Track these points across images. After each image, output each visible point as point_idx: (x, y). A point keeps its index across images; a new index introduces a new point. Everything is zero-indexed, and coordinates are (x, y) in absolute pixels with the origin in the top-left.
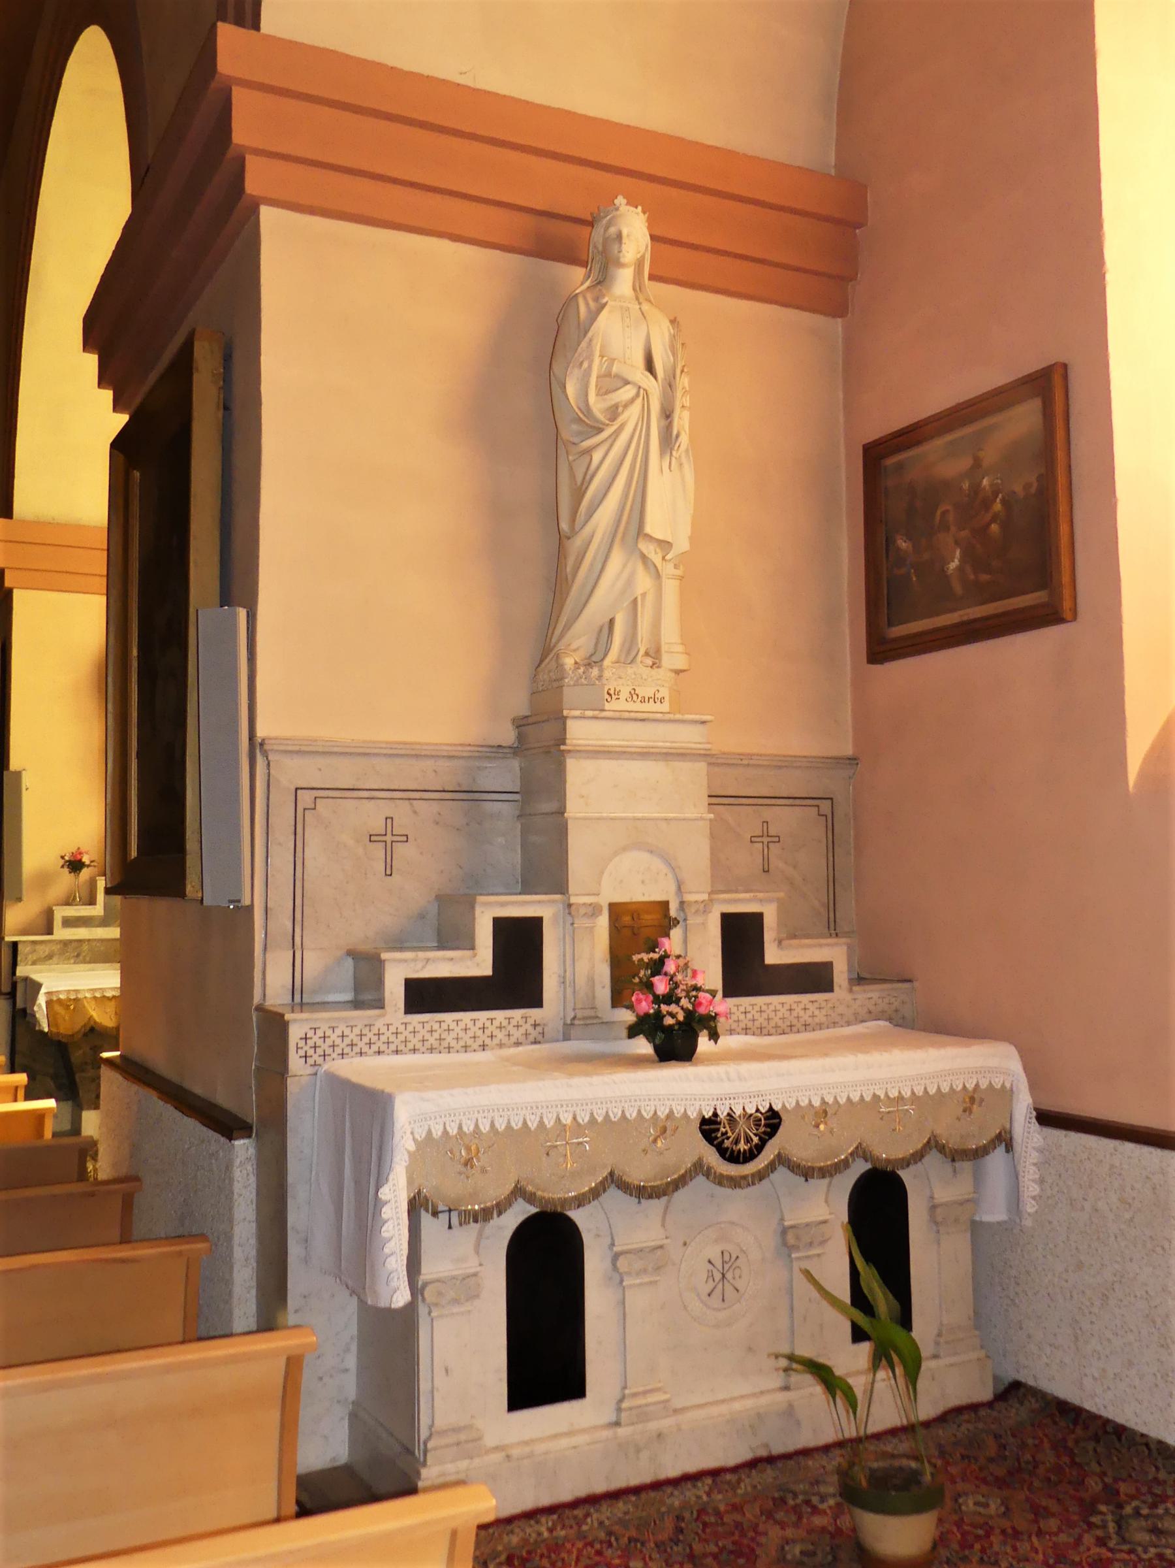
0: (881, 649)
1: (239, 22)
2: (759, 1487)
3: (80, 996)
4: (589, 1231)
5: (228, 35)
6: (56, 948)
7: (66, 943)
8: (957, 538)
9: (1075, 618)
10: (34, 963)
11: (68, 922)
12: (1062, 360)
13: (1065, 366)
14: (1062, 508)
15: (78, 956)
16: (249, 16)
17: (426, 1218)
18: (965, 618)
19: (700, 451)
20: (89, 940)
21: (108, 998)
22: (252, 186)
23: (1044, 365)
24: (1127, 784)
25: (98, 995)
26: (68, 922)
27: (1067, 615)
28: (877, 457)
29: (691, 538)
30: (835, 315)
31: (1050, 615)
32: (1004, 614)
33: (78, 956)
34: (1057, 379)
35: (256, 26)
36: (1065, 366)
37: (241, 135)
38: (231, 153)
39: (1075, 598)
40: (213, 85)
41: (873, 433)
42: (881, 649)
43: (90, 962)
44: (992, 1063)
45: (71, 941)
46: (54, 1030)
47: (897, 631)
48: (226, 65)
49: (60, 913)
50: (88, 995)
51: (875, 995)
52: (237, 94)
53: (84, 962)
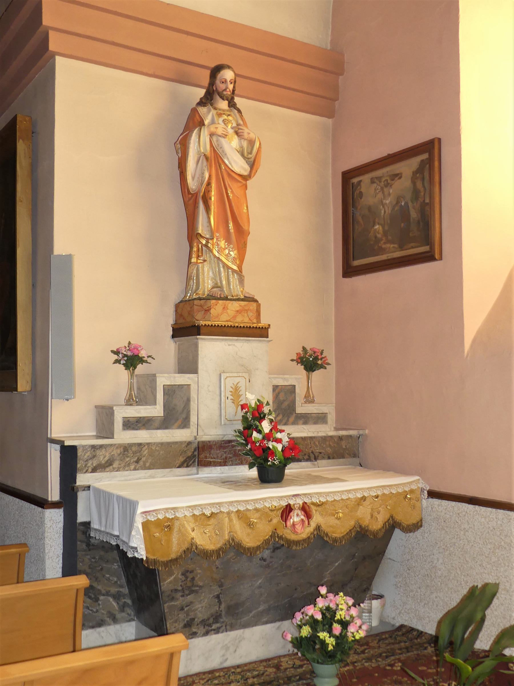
0: (349, 271)
3: (179, 515)
4: (243, 633)
6: (116, 452)
7: (126, 448)
8: (393, 215)
9: (441, 259)
10: (94, 470)
11: (131, 424)
13: (439, 140)
15: (137, 462)
18: (389, 258)
19: (281, 172)
20: (148, 444)
21: (324, 539)
23: (433, 138)
25: (197, 513)
26: (131, 424)
27: (437, 256)
30: (329, 117)
31: (429, 257)
32: (406, 256)
33: (137, 462)
38: (47, 55)
40: (40, 29)
42: (349, 271)
43: (149, 468)
45: (131, 445)
46: (151, 557)
49: (123, 412)
50: (188, 514)
52: (51, 34)
53: (144, 468)
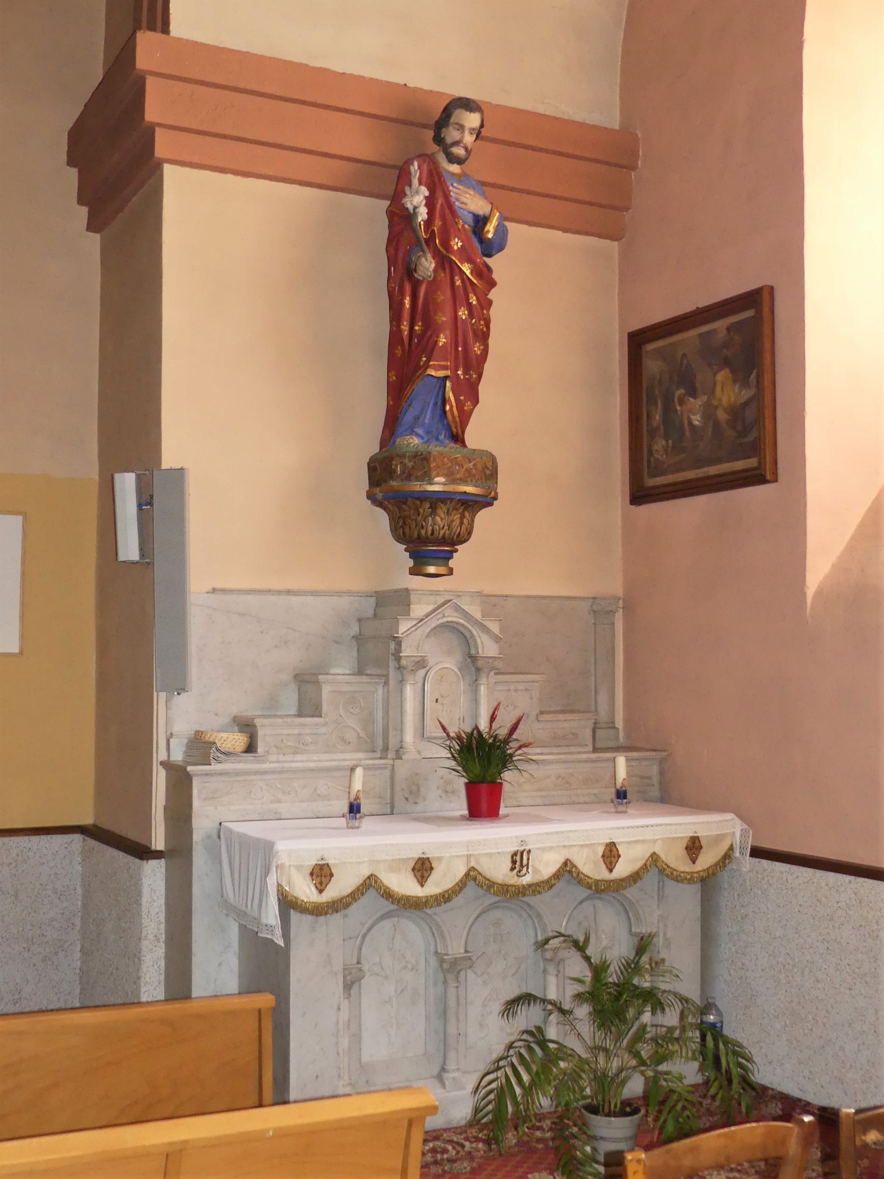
0: (640, 495)
1: (152, 28)
2: (225, 912)
5: (145, 40)
12: (769, 283)
13: (772, 288)
14: (767, 346)
16: (160, 21)
17: (294, 915)
22: (160, 151)
24: (806, 601)
28: (637, 341)
29: (427, 213)
31: (756, 477)
34: (765, 293)
35: (166, 30)
36: (772, 288)
37: (151, 114)
39: (773, 312)
41: (637, 324)
42: (640, 495)
44: (720, 828)
47: (651, 482)
48: (142, 62)
51: (452, 230)
